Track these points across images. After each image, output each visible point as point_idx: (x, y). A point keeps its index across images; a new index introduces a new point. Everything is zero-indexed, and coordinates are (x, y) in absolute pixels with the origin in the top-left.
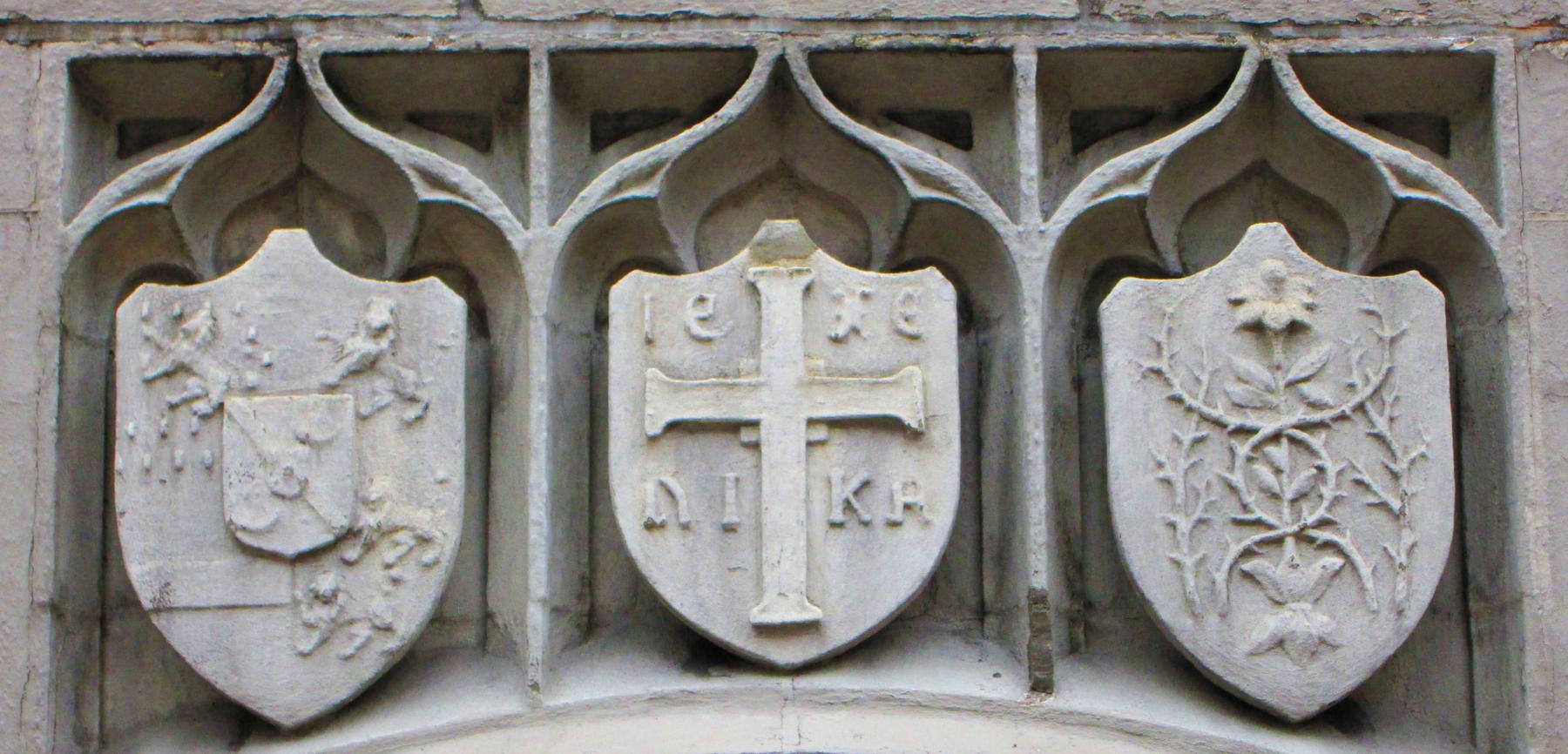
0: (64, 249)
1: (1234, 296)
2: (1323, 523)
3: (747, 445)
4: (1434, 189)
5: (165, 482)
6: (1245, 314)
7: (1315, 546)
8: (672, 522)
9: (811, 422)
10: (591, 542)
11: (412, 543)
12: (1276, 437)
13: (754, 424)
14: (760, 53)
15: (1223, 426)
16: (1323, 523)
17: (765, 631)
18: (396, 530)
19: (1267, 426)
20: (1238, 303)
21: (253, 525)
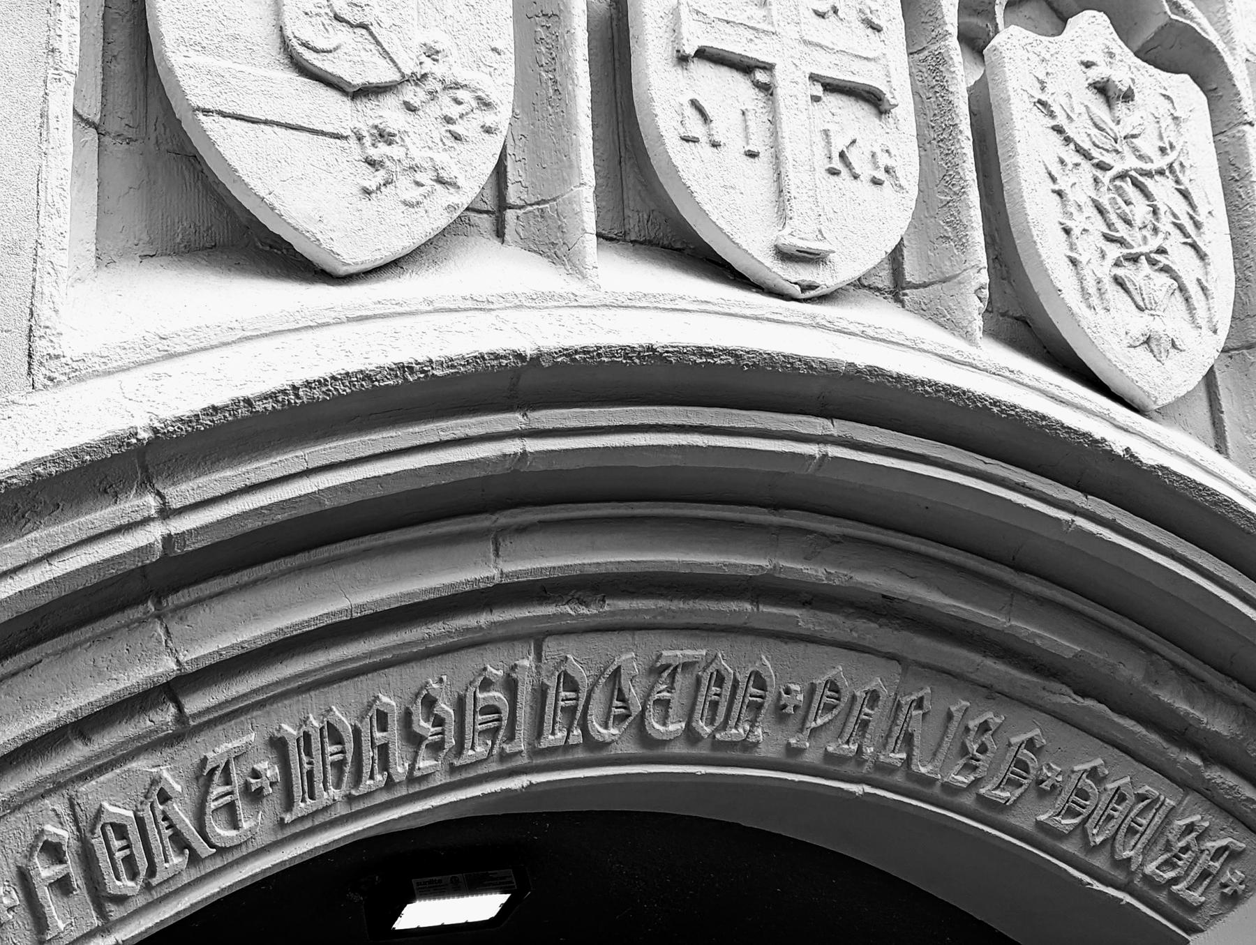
0: (886, 253)
1: (1085, 59)
2: (1161, 251)
3: (760, 86)
4: (1192, 19)
5: (797, 83)
6: (1095, 74)
7: (1156, 268)
8: (704, 139)
9: (814, 78)
10: (710, 313)
11: (474, 104)
12: (1122, 176)
13: (768, 68)
14: (121, 907)
15: (1091, 158)
16: (1161, 251)
17: (785, 256)
18: (457, 86)
19: (1118, 168)
20: (1088, 65)
21: (320, 45)
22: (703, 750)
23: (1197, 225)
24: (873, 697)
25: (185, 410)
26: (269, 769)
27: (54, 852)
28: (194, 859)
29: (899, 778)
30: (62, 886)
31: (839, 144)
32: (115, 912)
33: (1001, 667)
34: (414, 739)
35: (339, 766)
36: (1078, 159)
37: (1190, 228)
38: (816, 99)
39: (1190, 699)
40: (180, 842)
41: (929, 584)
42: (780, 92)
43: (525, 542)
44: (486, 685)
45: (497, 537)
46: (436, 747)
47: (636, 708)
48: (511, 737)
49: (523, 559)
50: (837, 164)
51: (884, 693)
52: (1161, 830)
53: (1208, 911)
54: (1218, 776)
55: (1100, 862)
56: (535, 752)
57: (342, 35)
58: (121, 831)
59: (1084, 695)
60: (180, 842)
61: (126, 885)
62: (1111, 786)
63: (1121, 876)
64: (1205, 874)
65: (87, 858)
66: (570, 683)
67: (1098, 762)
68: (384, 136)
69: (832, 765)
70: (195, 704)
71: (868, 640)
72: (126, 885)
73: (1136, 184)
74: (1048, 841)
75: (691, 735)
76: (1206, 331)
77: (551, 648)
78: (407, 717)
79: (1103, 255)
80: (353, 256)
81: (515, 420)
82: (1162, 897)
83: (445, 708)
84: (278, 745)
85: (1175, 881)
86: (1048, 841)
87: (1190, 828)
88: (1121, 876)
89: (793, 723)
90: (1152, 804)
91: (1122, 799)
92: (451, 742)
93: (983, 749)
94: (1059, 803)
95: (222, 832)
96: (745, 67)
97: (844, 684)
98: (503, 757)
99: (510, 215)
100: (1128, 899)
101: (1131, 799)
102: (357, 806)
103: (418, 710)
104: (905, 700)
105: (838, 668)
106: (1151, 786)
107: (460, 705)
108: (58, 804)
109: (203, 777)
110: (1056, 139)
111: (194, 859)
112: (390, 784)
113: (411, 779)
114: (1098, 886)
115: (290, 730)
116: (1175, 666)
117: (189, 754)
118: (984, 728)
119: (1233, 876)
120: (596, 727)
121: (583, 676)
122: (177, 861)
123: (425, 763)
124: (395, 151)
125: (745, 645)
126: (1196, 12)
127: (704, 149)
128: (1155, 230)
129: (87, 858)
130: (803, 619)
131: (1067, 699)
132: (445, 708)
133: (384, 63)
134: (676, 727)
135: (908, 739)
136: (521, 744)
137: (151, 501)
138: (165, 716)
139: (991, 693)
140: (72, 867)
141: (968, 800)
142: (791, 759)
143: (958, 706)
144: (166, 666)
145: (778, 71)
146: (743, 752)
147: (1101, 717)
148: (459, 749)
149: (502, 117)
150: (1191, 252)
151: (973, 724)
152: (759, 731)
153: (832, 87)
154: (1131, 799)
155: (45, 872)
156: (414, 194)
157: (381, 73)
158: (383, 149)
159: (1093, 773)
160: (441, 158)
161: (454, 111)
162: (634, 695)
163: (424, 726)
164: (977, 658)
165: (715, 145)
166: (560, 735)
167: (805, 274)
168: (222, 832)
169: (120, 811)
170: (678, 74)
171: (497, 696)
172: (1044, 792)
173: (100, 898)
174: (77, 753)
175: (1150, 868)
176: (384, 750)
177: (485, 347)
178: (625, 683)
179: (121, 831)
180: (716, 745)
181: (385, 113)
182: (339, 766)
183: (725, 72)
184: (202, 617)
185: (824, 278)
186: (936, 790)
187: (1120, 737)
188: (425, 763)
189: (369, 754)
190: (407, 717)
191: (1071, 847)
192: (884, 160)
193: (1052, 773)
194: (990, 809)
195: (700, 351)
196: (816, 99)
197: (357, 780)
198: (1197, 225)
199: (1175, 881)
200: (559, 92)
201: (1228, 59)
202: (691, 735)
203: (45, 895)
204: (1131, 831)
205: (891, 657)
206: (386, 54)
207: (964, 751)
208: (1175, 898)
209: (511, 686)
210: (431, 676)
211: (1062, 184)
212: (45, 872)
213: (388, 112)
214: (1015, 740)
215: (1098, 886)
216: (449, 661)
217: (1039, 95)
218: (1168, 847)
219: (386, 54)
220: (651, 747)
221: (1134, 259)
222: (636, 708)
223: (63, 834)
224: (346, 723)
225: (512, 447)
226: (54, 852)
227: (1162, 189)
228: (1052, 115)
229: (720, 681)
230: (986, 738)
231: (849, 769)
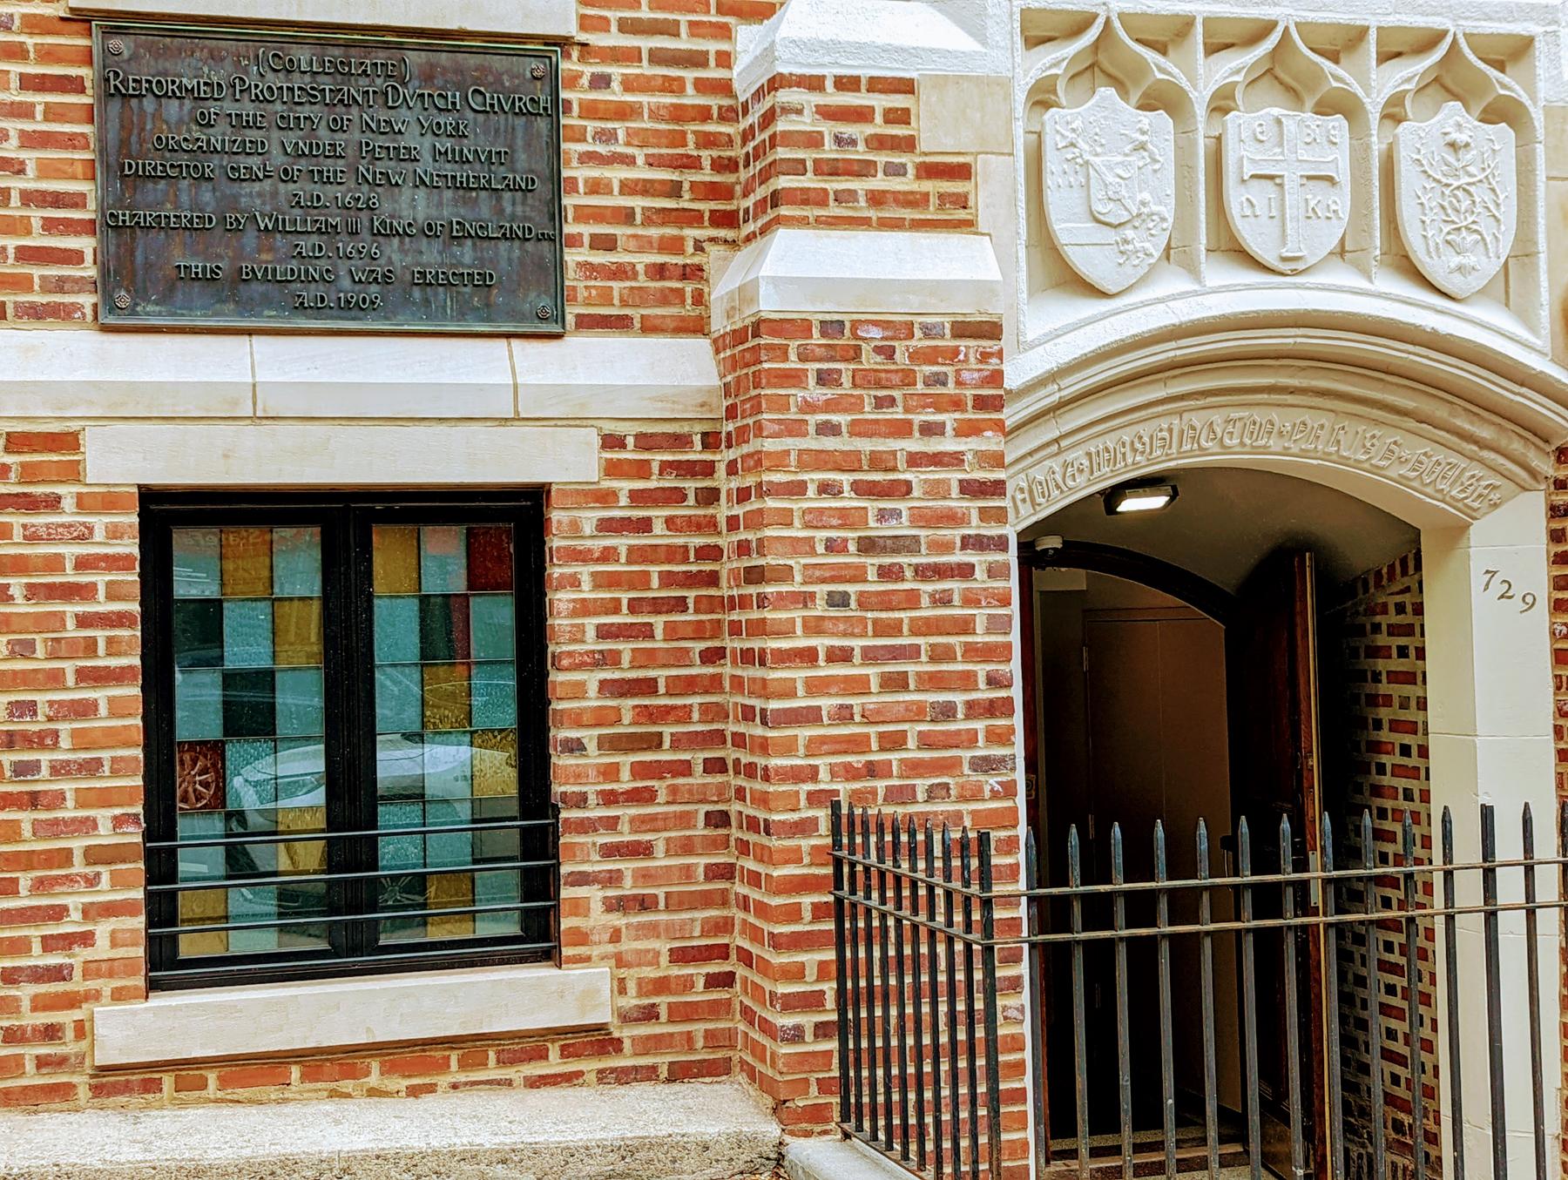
2: (1474, 222)
4: (1513, 91)
9: (1302, 176)
12: (1458, 188)
13: (1281, 177)
17: (1285, 259)
18: (1153, 214)
19: (1456, 184)
20: (1446, 134)
22: (1247, 449)
23: (1498, 205)
24: (1322, 427)
25: (1067, 360)
26: (1086, 463)
27: (1022, 490)
28: (1062, 492)
29: (1334, 457)
30: (1024, 500)
31: (1312, 204)
32: (1038, 508)
33: (1380, 413)
34: (1135, 451)
35: (1109, 460)
36: (1434, 185)
37: (1492, 207)
38: (1302, 185)
39: (1472, 423)
40: (1058, 487)
41: (1345, 382)
42: (1286, 187)
43: (1175, 381)
44: (1161, 430)
45: (1165, 381)
46: (1143, 453)
47: (1219, 436)
48: (1170, 448)
49: (1109, 1158)
50: (1311, 214)
51: (1327, 424)
52: (1459, 477)
53: (1481, 512)
54: (1486, 454)
55: (1429, 490)
56: (1179, 453)
57: (1111, 205)
58: (1041, 484)
59: (1421, 422)
60: (1058, 487)
61: (1041, 500)
62: (1434, 459)
63: (1439, 496)
64: (1480, 496)
65: (1031, 491)
66: (1194, 429)
67: (1428, 449)
68: (1126, 242)
69: (1304, 453)
70: (1063, 443)
71: (1320, 405)
72: (1041, 500)
73: (1464, 190)
74: (1404, 481)
75: (1242, 444)
76: (1494, 259)
77: (1185, 416)
78: (1132, 443)
79: (1441, 230)
80: (1114, 290)
81: (1173, 344)
82: (1460, 505)
83: (1146, 439)
84: (1089, 454)
85: (1466, 498)
86: (1404, 481)
87: (1473, 476)
88: (1439, 496)
89: (1287, 438)
90: (1453, 466)
91: (1440, 464)
92: (1148, 450)
93: (1373, 445)
94: (1409, 467)
95: (1071, 483)
96: (1272, 177)
97: (1309, 422)
98: (1167, 455)
99: (1172, 252)
100: (1443, 505)
101: (1443, 464)
102: (1114, 473)
103: (1136, 440)
104: (1337, 427)
105: (1307, 416)
106: (1454, 459)
107: (1151, 438)
108: (1023, 476)
109: (1066, 465)
110: (1423, 176)
111: (1062, 492)
112: (1126, 465)
113: (1133, 464)
114: (1428, 500)
115: (1093, 450)
116: (1465, 409)
117: (1060, 459)
118: (1373, 437)
119: (1495, 496)
120: (1203, 442)
121: (1198, 425)
122: (1057, 492)
123: (1138, 458)
124: (1130, 247)
125: (1263, 410)
126: (1517, 87)
127: (1252, 220)
128: (1473, 212)
129: (1031, 491)
130: (1290, 399)
131: (1412, 424)
132: (1146, 439)
133: (1125, 213)
134: (1236, 441)
135: (1339, 442)
136: (1174, 450)
137: (1056, 387)
138: (1055, 448)
139: (1377, 422)
140: (1026, 495)
141: (1366, 466)
142: (1286, 451)
143: (1361, 428)
144: (1057, 434)
145: (1286, 179)
146: (1265, 450)
147: (1429, 431)
148: (1151, 453)
149: (1168, 224)
150: (1492, 219)
151: (1368, 435)
152: (1271, 442)
153: (1309, 178)
154: (1443, 464)
155: (1019, 496)
156: (1136, 262)
157: (1125, 217)
158: (1127, 247)
159: (1425, 454)
160: (1147, 245)
161: (1151, 225)
162: (1219, 431)
163: (1138, 446)
164: (1369, 410)
165: (1256, 216)
166: (1189, 446)
167: (1293, 266)
168: (1071, 483)
169: (1041, 478)
170: (1242, 189)
171: (1165, 434)
172: (1402, 461)
173: (1034, 504)
174: (1030, 460)
175: (1454, 493)
176: (1124, 454)
177: (1162, 324)
178: (1215, 427)
179: (1041, 484)
180: (1253, 447)
181: (1127, 232)
182: (1109, 460)
183: (1263, 181)
184: (1067, 417)
185: (1300, 266)
186: (1351, 462)
187: (1438, 439)
188: (1138, 458)
189: (1119, 456)
190: (1132, 443)
191: (1415, 484)
192: (1333, 207)
193: (1405, 454)
194: (1376, 469)
195: (1243, 313)
196: (1302, 185)
197: (1115, 465)
198: (1498, 205)
199: (1466, 498)
200: (1193, 199)
201: (1531, 109)
202: (1242, 444)
203: (1019, 503)
204: (1443, 477)
205: (1332, 411)
206: (1126, 209)
207: (1364, 446)
208: (1466, 505)
209: (1170, 431)
210: (1140, 428)
211: (1423, 200)
212: (1019, 496)
213: (1129, 233)
214: (1388, 441)
215: (1428, 500)
216: (1148, 423)
217: (1415, 156)
218: (1462, 484)
219: (1126, 209)
220: (1226, 449)
221: (1459, 229)
222: (1219, 436)
223: (1024, 485)
224: (1111, 446)
225: (1171, 354)
226: (1022, 490)
227: (1481, 193)
228: (1422, 165)
229: (1255, 423)
230: (1374, 441)
231: (1312, 455)
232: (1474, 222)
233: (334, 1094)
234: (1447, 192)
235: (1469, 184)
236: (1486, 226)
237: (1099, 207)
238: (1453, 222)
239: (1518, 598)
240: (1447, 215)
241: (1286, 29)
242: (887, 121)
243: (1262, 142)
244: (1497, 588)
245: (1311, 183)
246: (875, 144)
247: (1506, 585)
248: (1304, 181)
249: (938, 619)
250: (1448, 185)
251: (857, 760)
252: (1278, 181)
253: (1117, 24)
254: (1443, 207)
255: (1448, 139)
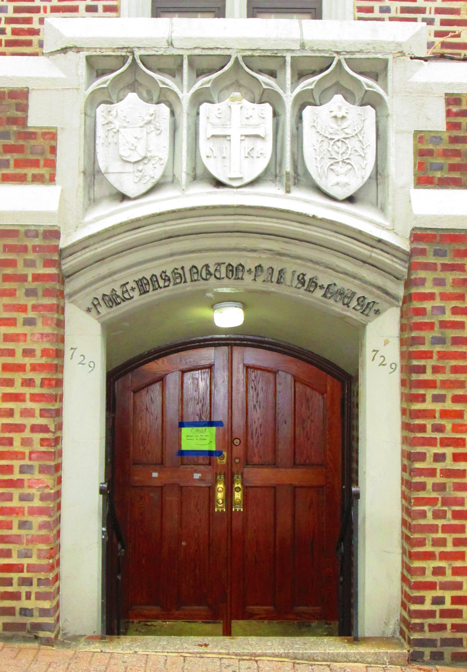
2: (348, 159)
4: (374, 88)
12: (338, 141)
13: (230, 136)
17: (231, 179)
73: (342, 141)
96: (225, 136)
153: (246, 136)
232: (348, 159)
233: (388, 186)
234: (332, 143)
235: (345, 138)
236: (354, 160)
237: (123, 153)
238: (334, 158)
239: (388, 365)
240: (331, 155)
241: (237, 58)
242: (15, 319)
243: (220, 118)
244: (378, 360)
245: (247, 139)
246: (27, 612)
247: (382, 358)
248: (243, 138)
249: (12, 459)
250: (332, 139)
251: (448, 40)
252: (228, 138)
253: (139, 61)
254: (329, 151)
255: (333, 114)
